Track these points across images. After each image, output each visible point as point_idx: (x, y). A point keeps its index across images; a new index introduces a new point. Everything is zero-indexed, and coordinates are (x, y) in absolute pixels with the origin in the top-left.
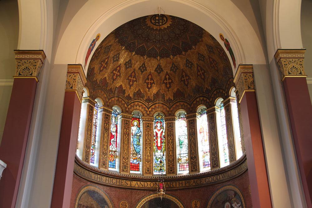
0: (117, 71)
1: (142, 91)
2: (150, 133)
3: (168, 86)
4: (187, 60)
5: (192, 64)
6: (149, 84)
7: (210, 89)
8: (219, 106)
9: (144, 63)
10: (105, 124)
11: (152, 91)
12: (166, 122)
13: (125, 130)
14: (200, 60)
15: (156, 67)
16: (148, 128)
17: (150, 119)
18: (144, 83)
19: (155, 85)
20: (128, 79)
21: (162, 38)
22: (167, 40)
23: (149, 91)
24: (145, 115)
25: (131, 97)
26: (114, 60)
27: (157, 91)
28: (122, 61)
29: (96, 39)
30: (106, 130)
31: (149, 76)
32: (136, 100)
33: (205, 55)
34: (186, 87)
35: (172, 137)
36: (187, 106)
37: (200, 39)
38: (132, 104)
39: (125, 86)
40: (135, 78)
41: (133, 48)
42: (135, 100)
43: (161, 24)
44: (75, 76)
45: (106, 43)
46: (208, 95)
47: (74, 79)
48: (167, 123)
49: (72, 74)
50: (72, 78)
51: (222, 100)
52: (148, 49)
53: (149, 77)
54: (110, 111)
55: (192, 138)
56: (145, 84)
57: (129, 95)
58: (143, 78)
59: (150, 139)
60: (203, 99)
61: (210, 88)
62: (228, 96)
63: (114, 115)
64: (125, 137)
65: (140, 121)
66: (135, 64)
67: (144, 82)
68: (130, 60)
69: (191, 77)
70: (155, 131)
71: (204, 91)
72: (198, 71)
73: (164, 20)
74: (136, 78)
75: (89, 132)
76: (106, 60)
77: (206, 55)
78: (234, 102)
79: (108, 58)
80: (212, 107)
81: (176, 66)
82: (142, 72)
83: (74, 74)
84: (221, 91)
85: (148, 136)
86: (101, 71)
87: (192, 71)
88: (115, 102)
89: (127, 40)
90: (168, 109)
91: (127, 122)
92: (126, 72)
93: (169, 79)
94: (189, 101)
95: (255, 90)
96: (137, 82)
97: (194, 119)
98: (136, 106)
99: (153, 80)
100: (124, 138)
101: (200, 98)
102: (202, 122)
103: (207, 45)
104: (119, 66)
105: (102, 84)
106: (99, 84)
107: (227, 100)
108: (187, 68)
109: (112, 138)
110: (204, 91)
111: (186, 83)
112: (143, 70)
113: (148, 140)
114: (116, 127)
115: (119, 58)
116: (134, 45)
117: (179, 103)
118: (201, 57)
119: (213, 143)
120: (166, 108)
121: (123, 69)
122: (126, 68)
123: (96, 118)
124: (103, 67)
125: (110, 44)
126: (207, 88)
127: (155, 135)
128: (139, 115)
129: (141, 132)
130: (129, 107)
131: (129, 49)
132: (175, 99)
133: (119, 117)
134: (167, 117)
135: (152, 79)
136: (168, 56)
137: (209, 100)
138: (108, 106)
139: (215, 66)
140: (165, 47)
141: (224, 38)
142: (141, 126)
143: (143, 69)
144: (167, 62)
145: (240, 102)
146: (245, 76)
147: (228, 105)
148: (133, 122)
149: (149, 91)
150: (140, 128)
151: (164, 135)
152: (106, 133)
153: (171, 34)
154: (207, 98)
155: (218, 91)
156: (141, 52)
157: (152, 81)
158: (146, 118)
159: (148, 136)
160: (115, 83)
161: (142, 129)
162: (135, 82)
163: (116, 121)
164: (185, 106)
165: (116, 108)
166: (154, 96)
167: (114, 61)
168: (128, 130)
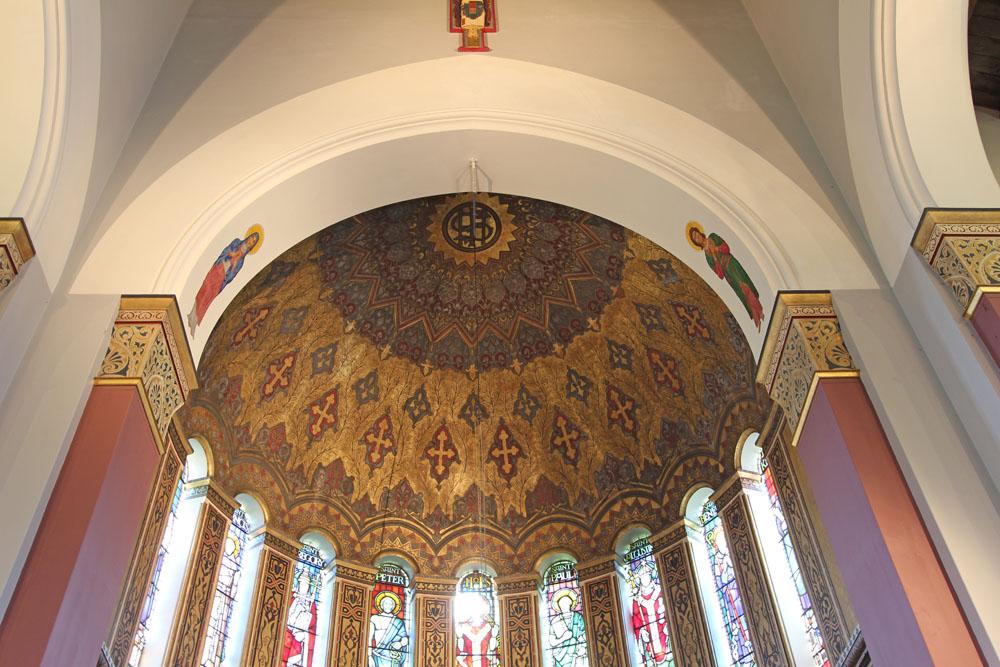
0: (327, 407)
1: (413, 485)
2: (442, 635)
3: (507, 467)
4: (571, 372)
5: (590, 384)
6: (440, 461)
7: (660, 464)
8: (699, 522)
9: (423, 386)
10: (269, 593)
11: (449, 489)
12: (503, 597)
13: (346, 622)
14: (615, 366)
15: (465, 401)
16: (434, 616)
17: (441, 587)
18: (422, 459)
19: (462, 467)
20: (366, 441)
21: (484, 298)
22: (501, 305)
23: (439, 488)
24: (425, 570)
25: (375, 505)
26: (314, 365)
27: (466, 488)
28: (343, 374)
29: (247, 239)
30: (270, 616)
31: (438, 433)
32: (392, 519)
33: (633, 346)
34: (572, 467)
35: (528, 652)
36: (577, 534)
37: (612, 288)
38: (377, 532)
39: (355, 465)
40: (388, 440)
41: (382, 331)
42: (390, 515)
43: (478, 244)
44: (144, 334)
45: (288, 295)
46: (651, 486)
47: (137, 344)
48: (506, 598)
49: (134, 327)
50: (130, 340)
51: (709, 491)
52: (434, 339)
53: (439, 437)
54: (293, 547)
55: (606, 649)
56: (426, 461)
57: (366, 496)
58: (419, 442)
59: (443, 658)
60: (636, 503)
61: (658, 460)
62: (732, 468)
63: (306, 569)
64: (343, 647)
65: (404, 595)
66: (389, 391)
67: (420, 456)
68: (373, 374)
69: (588, 431)
70: (460, 631)
71: (639, 476)
72: (613, 406)
73: (489, 227)
74: (392, 440)
75: (196, 608)
76: (288, 362)
77: (637, 341)
78: (757, 490)
79: (294, 355)
80: (670, 523)
81: (532, 398)
82: (415, 419)
83: (139, 328)
84: (702, 460)
85: (435, 649)
86: (265, 397)
87: (590, 411)
88: (315, 519)
89: (362, 297)
90: (508, 550)
91: (357, 594)
92: (357, 416)
93: (511, 443)
94: (584, 516)
95: (858, 371)
96: (395, 454)
97: (609, 577)
98: (393, 538)
99: (455, 450)
100: (342, 654)
101: (623, 503)
102: (639, 586)
103: (638, 306)
104: (334, 392)
105: (268, 445)
106: (254, 445)
107: (729, 484)
108: (573, 399)
109: (293, 651)
110: (639, 476)
111: (571, 453)
112: (416, 413)
113: (435, 661)
114: (314, 611)
115: (333, 363)
116: (388, 321)
117: (547, 527)
118: (617, 356)
119: (693, 657)
120: (502, 547)
121: (347, 405)
122: (360, 402)
123: (234, 567)
124: (273, 382)
125: (303, 302)
126: (646, 461)
127: (461, 648)
128: (400, 574)
129: (408, 637)
130: (367, 538)
131: (369, 332)
132: (533, 514)
133: (327, 577)
134: (508, 579)
135: (448, 445)
136: (504, 365)
137: (660, 503)
138: (285, 528)
139: (670, 376)
140: (492, 328)
141: (703, 236)
142: (409, 614)
143: (419, 409)
144: (500, 384)
145: (794, 444)
146: (809, 329)
147: (738, 502)
148: (378, 599)
149: (439, 488)
150: (403, 620)
151: (496, 649)
152: (269, 625)
153: (515, 281)
154: (652, 497)
155: (690, 465)
156: (412, 352)
157: (450, 454)
158: (427, 580)
159: (435, 649)
160: (316, 450)
161: (410, 624)
162: (390, 454)
163: (313, 590)
164: (570, 536)
165: (316, 545)
166: (456, 503)
167: (316, 371)
168: (356, 624)
